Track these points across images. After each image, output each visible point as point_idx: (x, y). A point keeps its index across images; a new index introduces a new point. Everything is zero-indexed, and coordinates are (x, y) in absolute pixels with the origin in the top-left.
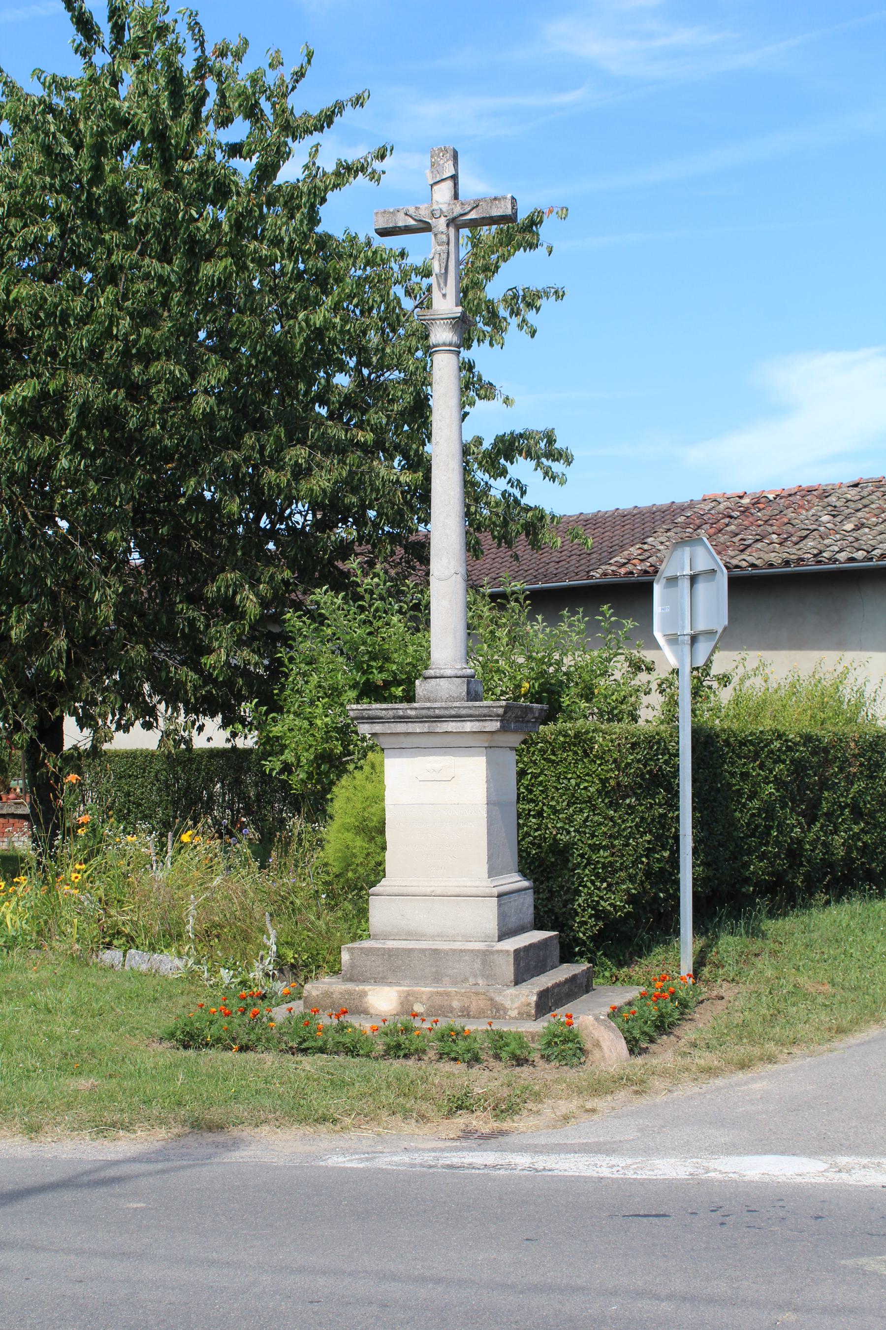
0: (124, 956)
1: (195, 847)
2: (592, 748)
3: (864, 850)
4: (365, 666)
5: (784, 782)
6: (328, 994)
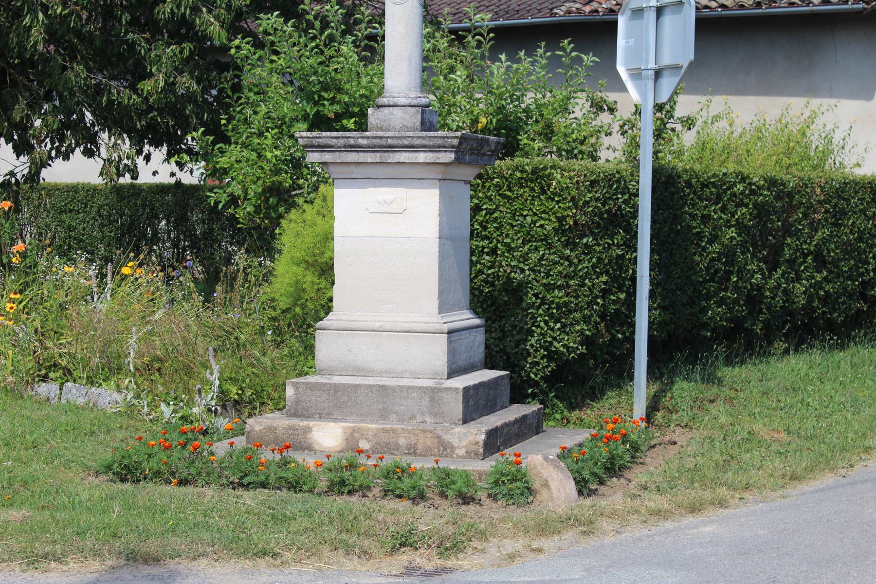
0: (61, 389)
1: (137, 279)
2: (549, 185)
3: (826, 299)
4: (316, 97)
5: (746, 227)
6: (271, 429)
